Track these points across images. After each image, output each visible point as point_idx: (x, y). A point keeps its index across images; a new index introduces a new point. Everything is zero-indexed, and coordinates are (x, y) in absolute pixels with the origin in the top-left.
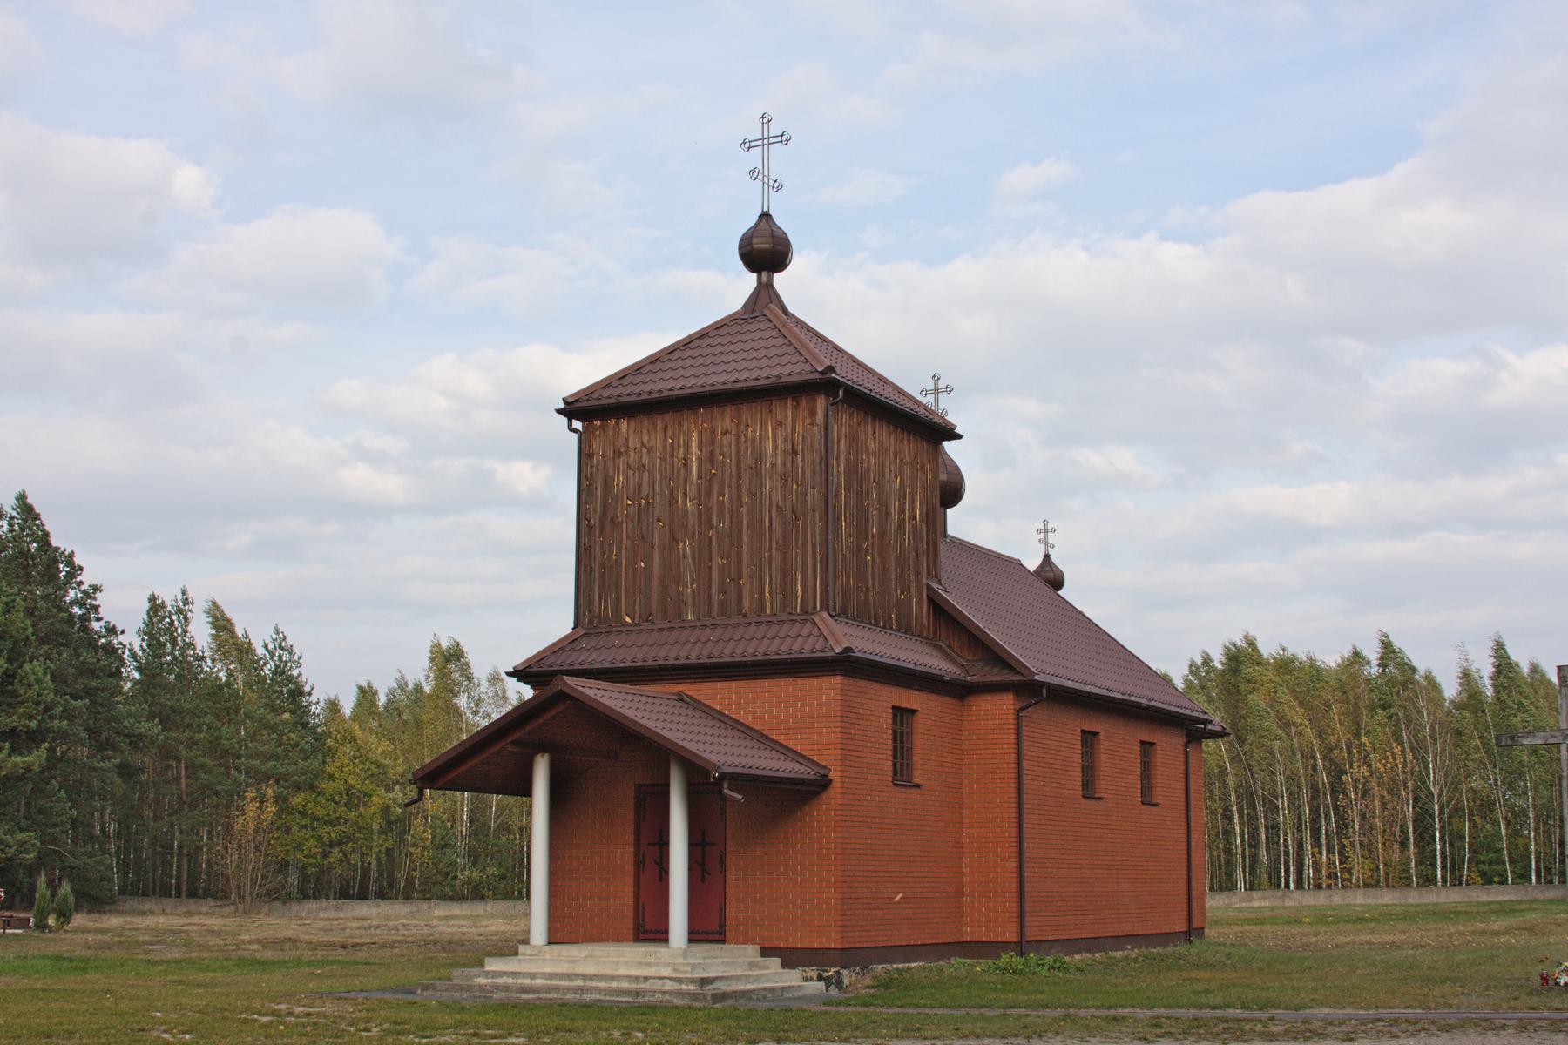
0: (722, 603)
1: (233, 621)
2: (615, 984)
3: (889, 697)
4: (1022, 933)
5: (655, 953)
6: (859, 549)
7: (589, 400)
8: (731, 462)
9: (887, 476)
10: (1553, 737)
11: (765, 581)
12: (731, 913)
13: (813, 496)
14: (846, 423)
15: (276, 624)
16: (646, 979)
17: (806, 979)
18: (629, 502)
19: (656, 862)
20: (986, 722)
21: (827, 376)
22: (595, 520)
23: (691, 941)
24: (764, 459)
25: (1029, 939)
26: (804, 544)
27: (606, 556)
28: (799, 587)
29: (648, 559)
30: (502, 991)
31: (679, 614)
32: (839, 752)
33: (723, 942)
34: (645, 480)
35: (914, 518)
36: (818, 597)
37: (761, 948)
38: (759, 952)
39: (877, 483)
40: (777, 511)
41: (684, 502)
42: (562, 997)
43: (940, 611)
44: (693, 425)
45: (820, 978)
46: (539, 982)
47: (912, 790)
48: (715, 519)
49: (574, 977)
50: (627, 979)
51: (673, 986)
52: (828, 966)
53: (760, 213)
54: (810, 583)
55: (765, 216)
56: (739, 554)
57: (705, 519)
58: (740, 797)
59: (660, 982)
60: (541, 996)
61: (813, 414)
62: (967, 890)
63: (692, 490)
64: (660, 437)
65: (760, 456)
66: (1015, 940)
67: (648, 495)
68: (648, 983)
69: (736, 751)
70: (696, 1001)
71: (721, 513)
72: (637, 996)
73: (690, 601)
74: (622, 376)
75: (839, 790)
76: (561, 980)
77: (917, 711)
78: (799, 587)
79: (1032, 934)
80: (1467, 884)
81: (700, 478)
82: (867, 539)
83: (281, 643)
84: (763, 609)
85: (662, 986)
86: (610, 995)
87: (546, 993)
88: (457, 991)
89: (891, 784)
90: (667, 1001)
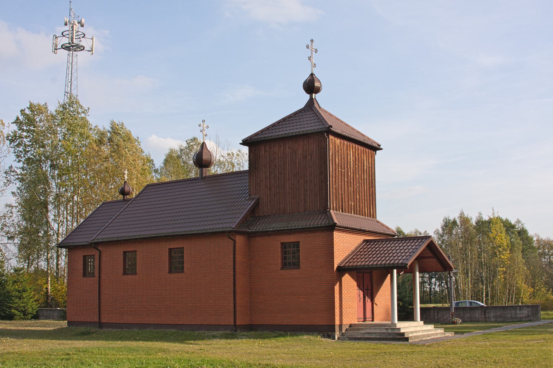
1: (134, 135)
7: (251, 140)
15: (30, 101)
55: (312, 75)
74: (262, 131)
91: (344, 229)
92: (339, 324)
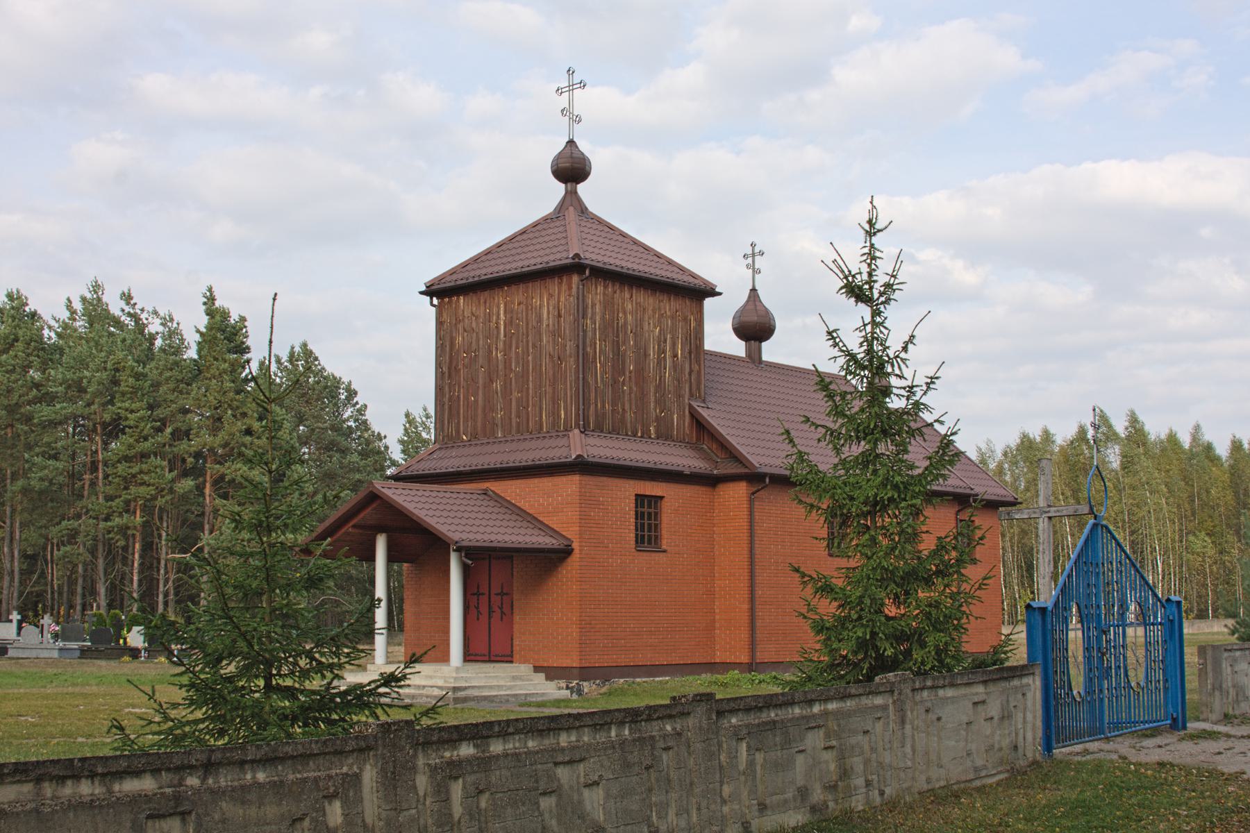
0: (518, 424)
3: (630, 489)
4: (753, 656)
6: (615, 382)
9: (646, 327)
10: (1035, 513)
12: (516, 642)
13: (570, 347)
14: (598, 293)
16: (424, 687)
17: (560, 688)
25: (758, 661)
26: (566, 382)
28: (562, 412)
29: (476, 395)
31: (493, 434)
32: (578, 528)
33: (511, 662)
35: (675, 356)
38: (532, 669)
39: (635, 333)
41: (497, 354)
43: (700, 426)
45: (568, 688)
47: (661, 554)
53: (567, 140)
54: (569, 409)
55: (571, 142)
56: (528, 389)
57: (507, 363)
58: (470, 562)
61: (570, 288)
62: (717, 625)
64: (482, 308)
65: (540, 320)
66: (747, 661)
69: (516, 531)
71: (517, 363)
75: (578, 556)
77: (663, 497)
78: (562, 412)
79: (759, 657)
81: (505, 336)
82: (624, 374)
84: (541, 428)
89: (634, 550)
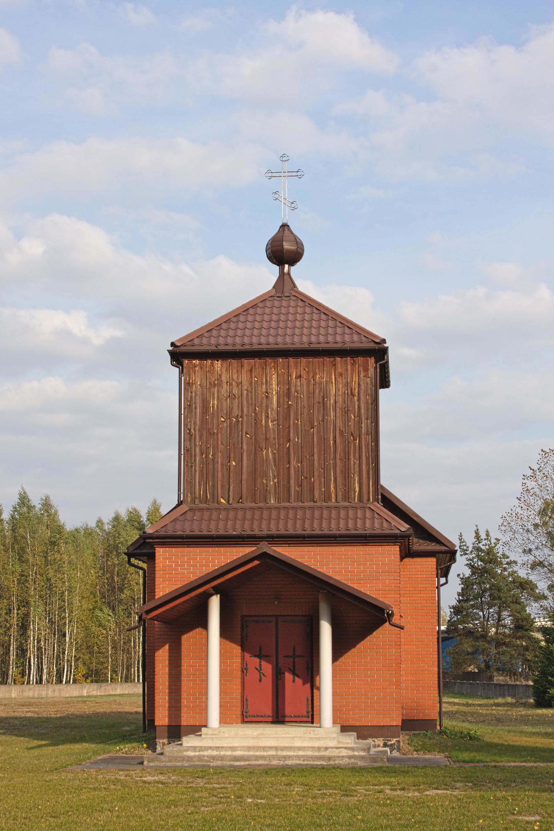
2: (301, 753)
5: (314, 731)
8: (304, 396)
11: (330, 480)
16: (326, 748)
18: (223, 420)
19: (256, 669)
20: (416, 576)
21: (381, 346)
22: (195, 430)
23: (333, 723)
24: (329, 398)
27: (204, 456)
30: (218, 760)
34: (236, 404)
36: (371, 492)
37: (341, 726)
40: (340, 433)
42: (269, 763)
44: (273, 370)
46: (238, 753)
48: (292, 435)
49: (267, 749)
50: (311, 749)
51: (347, 753)
52: (391, 738)
59: (337, 751)
60: (251, 763)
61: (366, 370)
63: (272, 414)
65: (325, 396)
67: (237, 416)
68: (328, 751)
70: (375, 763)
72: (329, 761)
73: (273, 490)
76: (257, 751)
80: (111, 681)
83: (47, 505)
85: (339, 753)
86: (307, 760)
87: (255, 760)
88: (179, 761)
90: (353, 763)
91: (181, 540)
92: (166, 722)
